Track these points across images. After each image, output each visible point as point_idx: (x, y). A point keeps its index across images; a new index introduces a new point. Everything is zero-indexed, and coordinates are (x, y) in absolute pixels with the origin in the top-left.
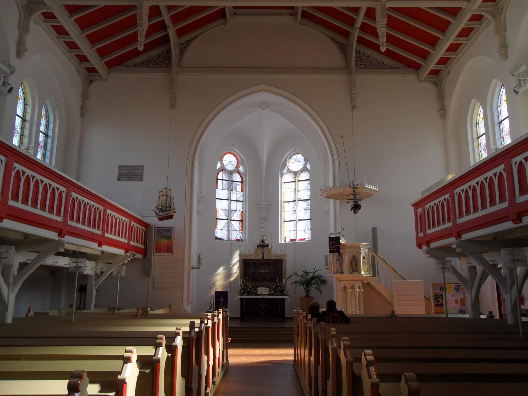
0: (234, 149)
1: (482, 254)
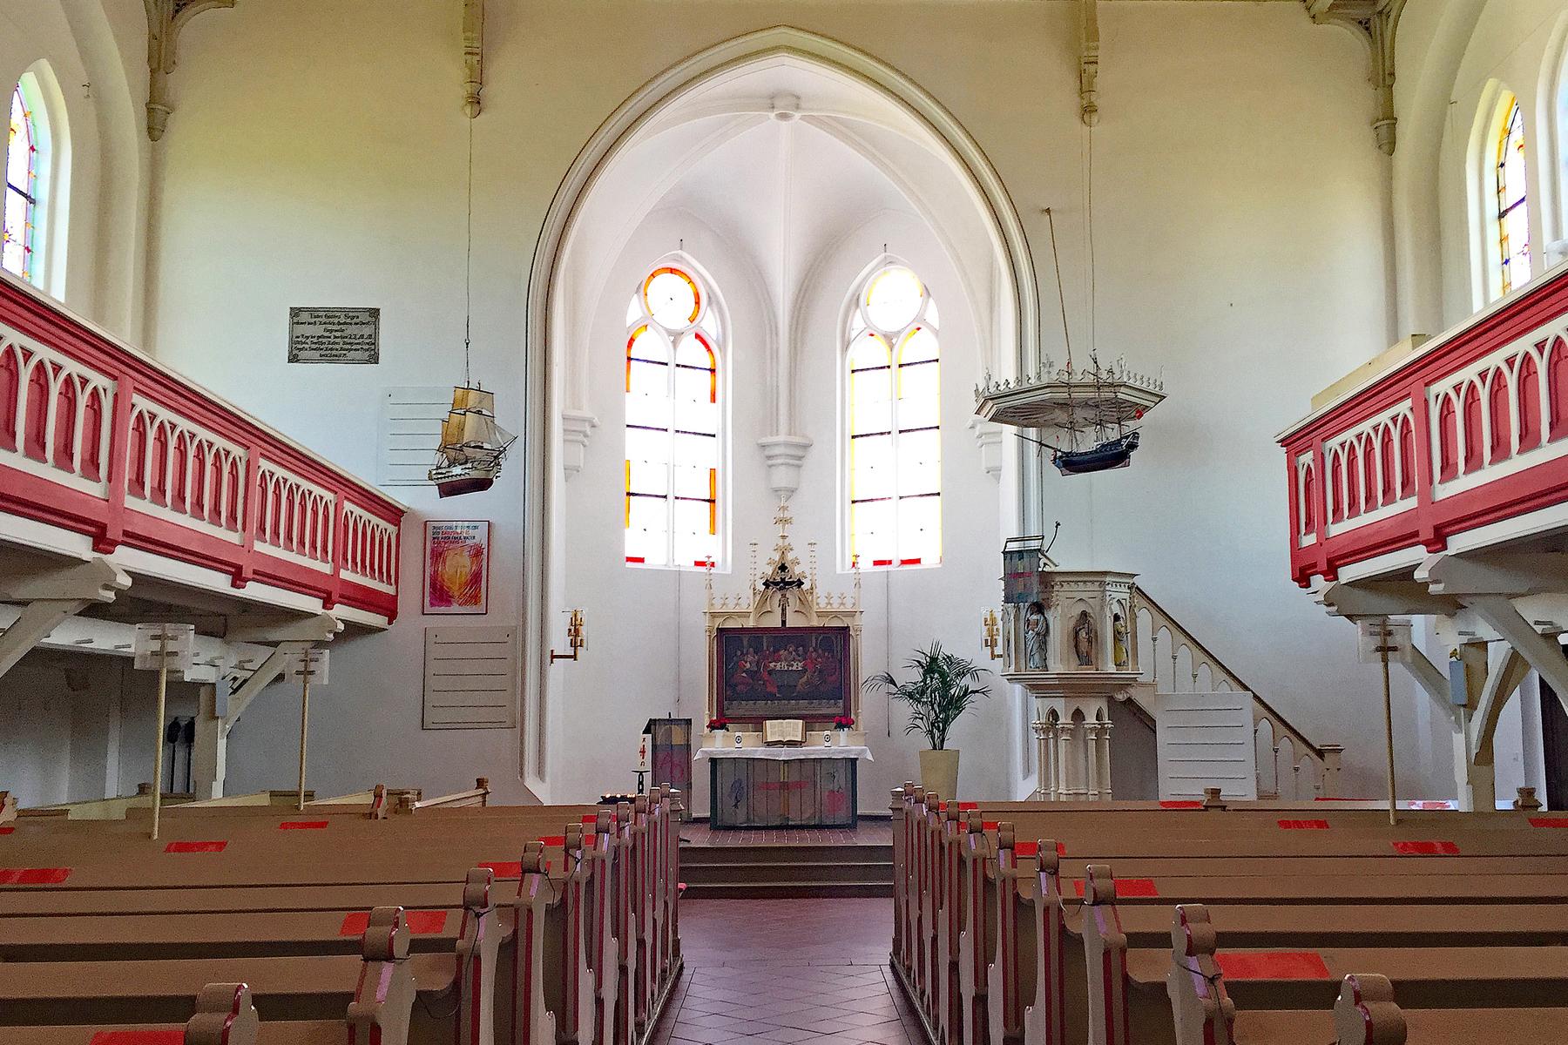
0: (685, 255)
1: (1513, 601)
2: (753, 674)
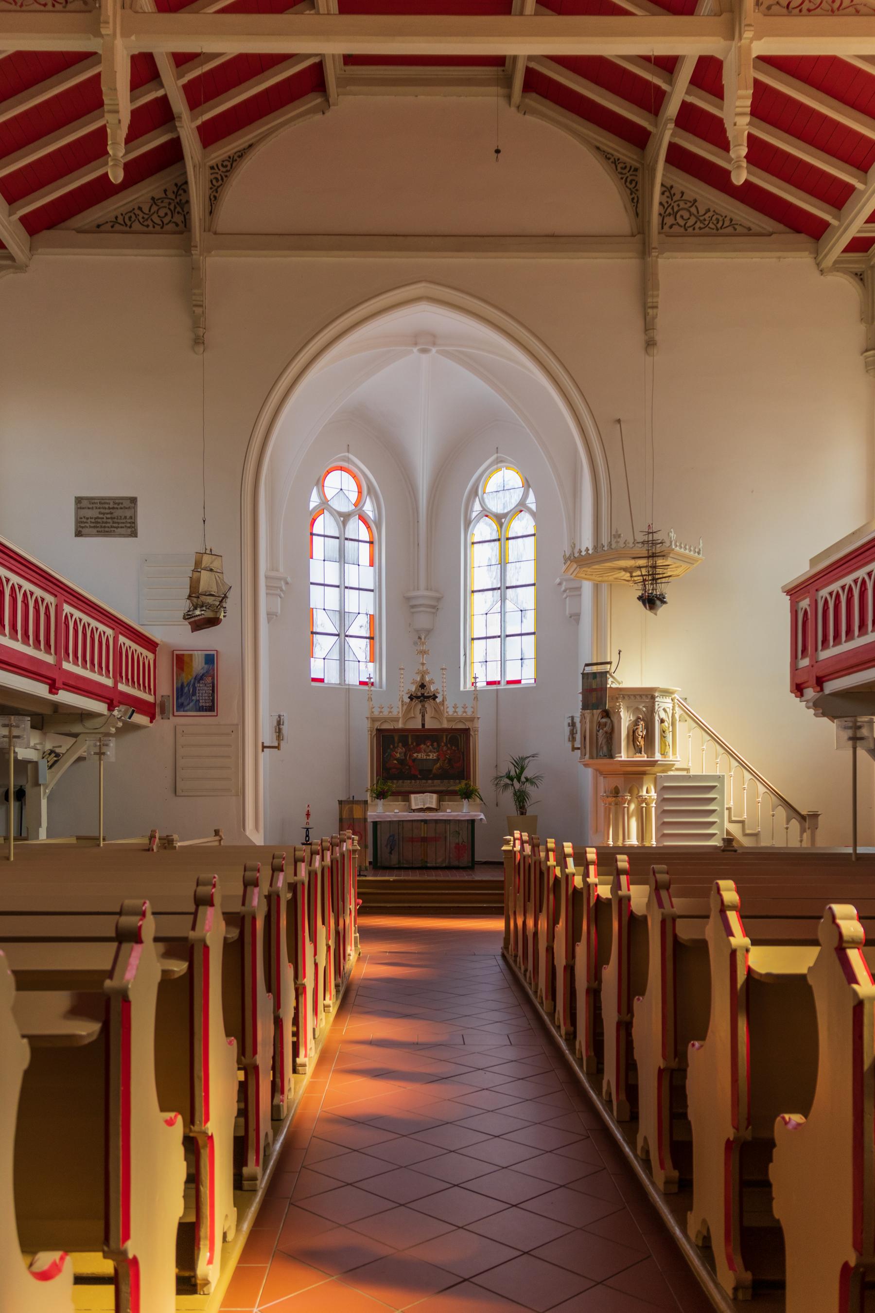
0: (351, 456)
2: (401, 762)
